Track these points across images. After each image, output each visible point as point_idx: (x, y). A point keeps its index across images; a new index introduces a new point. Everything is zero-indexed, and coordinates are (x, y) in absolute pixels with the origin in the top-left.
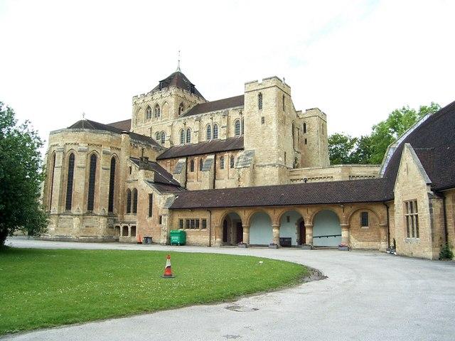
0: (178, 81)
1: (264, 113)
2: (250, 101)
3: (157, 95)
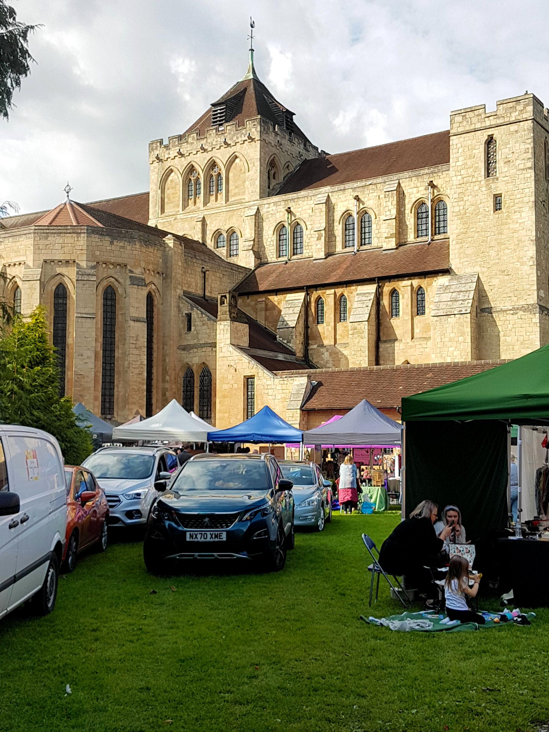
0: (247, 102)
1: (500, 187)
2: (465, 152)
3: (213, 138)
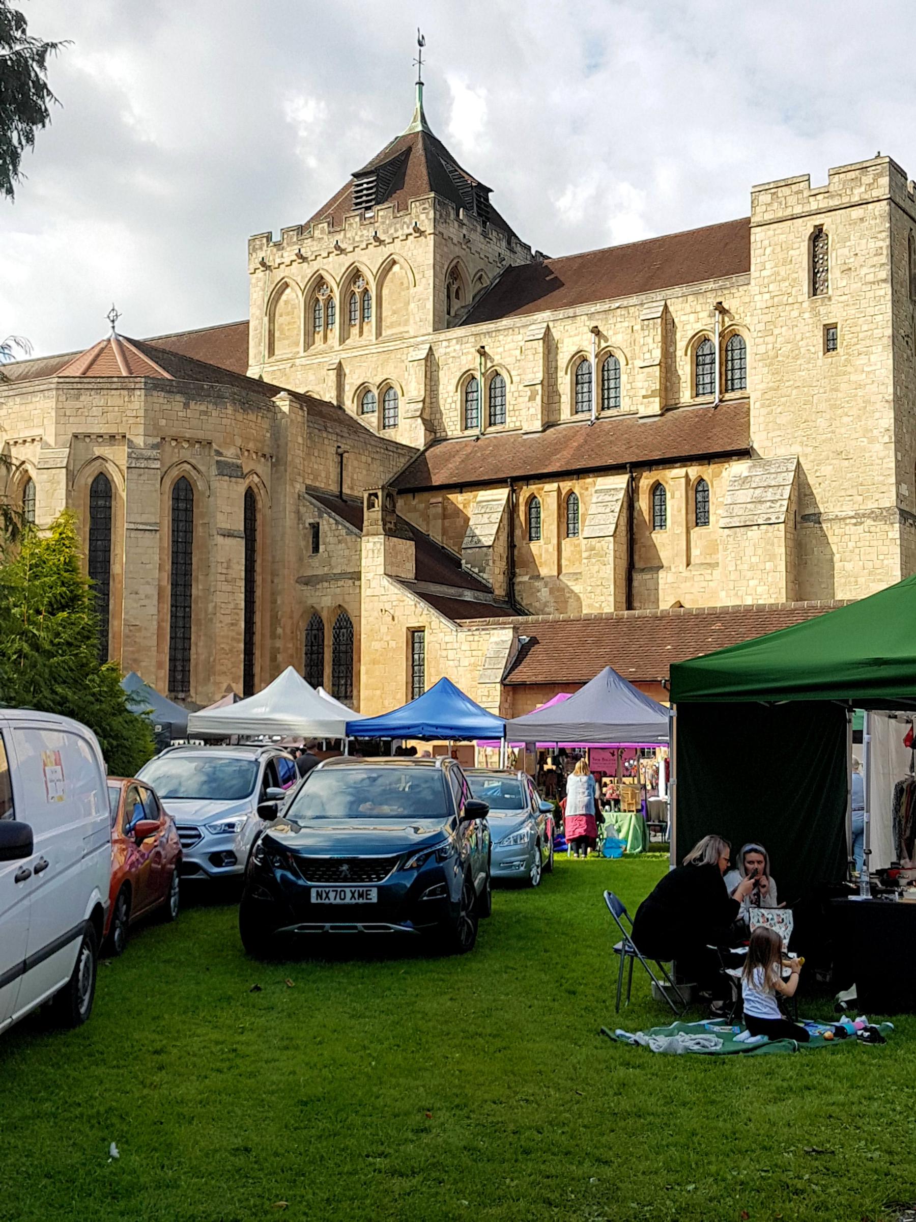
0: (412, 170)
1: (834, 312)
2: (776, 254)
3: (355, 231)
